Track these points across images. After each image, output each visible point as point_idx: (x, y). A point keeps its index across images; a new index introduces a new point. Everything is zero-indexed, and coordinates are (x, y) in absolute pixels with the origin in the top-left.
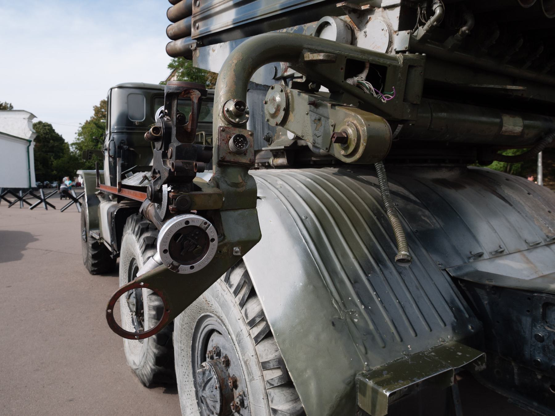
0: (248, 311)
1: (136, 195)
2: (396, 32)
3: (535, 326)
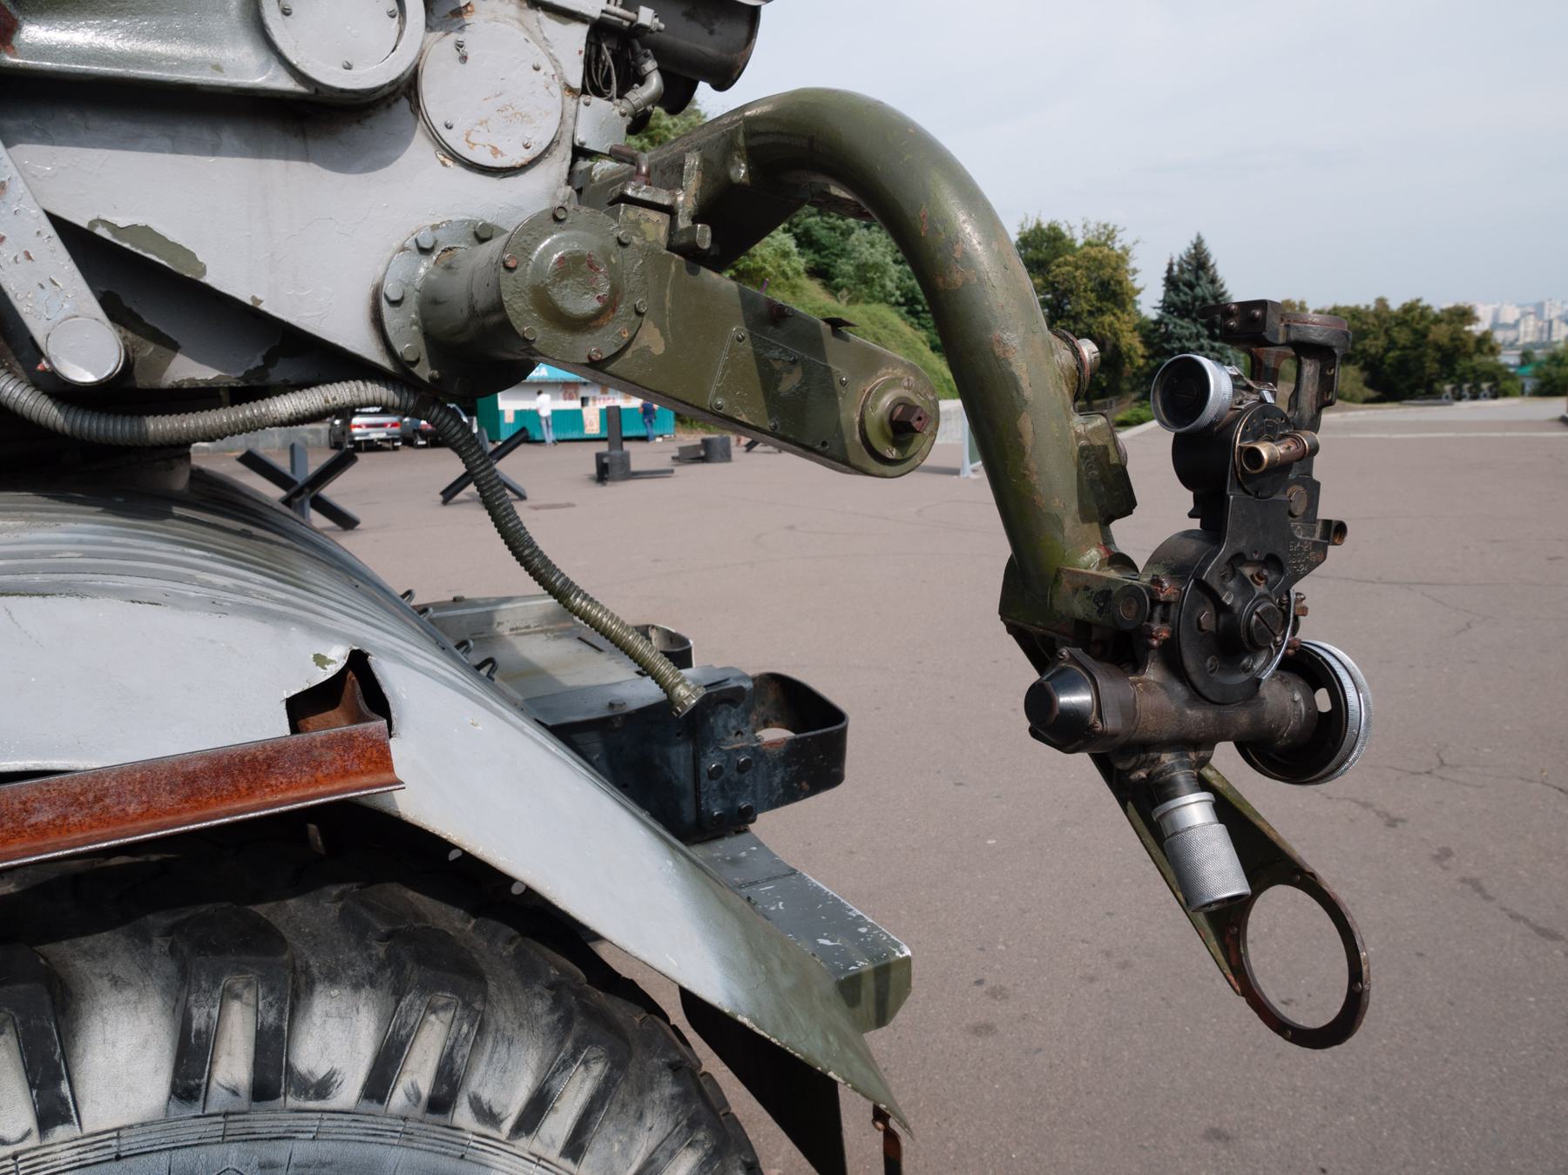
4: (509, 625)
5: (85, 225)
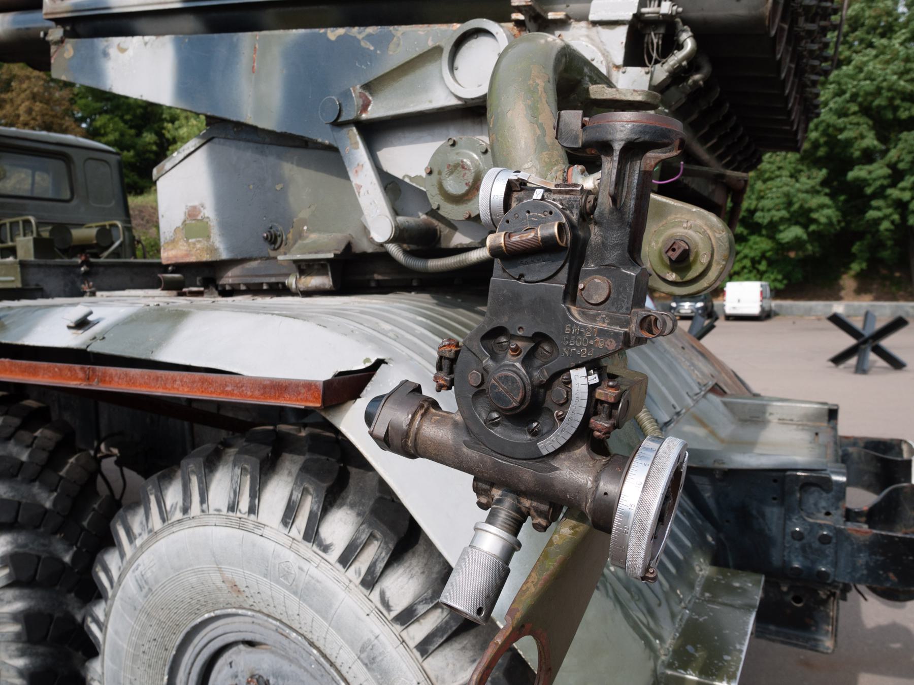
0: (388, 594)
1: (61, 375)
2: (618, 67)
3: (790, 519)
4: (779, 416)
5: (401, 177)
